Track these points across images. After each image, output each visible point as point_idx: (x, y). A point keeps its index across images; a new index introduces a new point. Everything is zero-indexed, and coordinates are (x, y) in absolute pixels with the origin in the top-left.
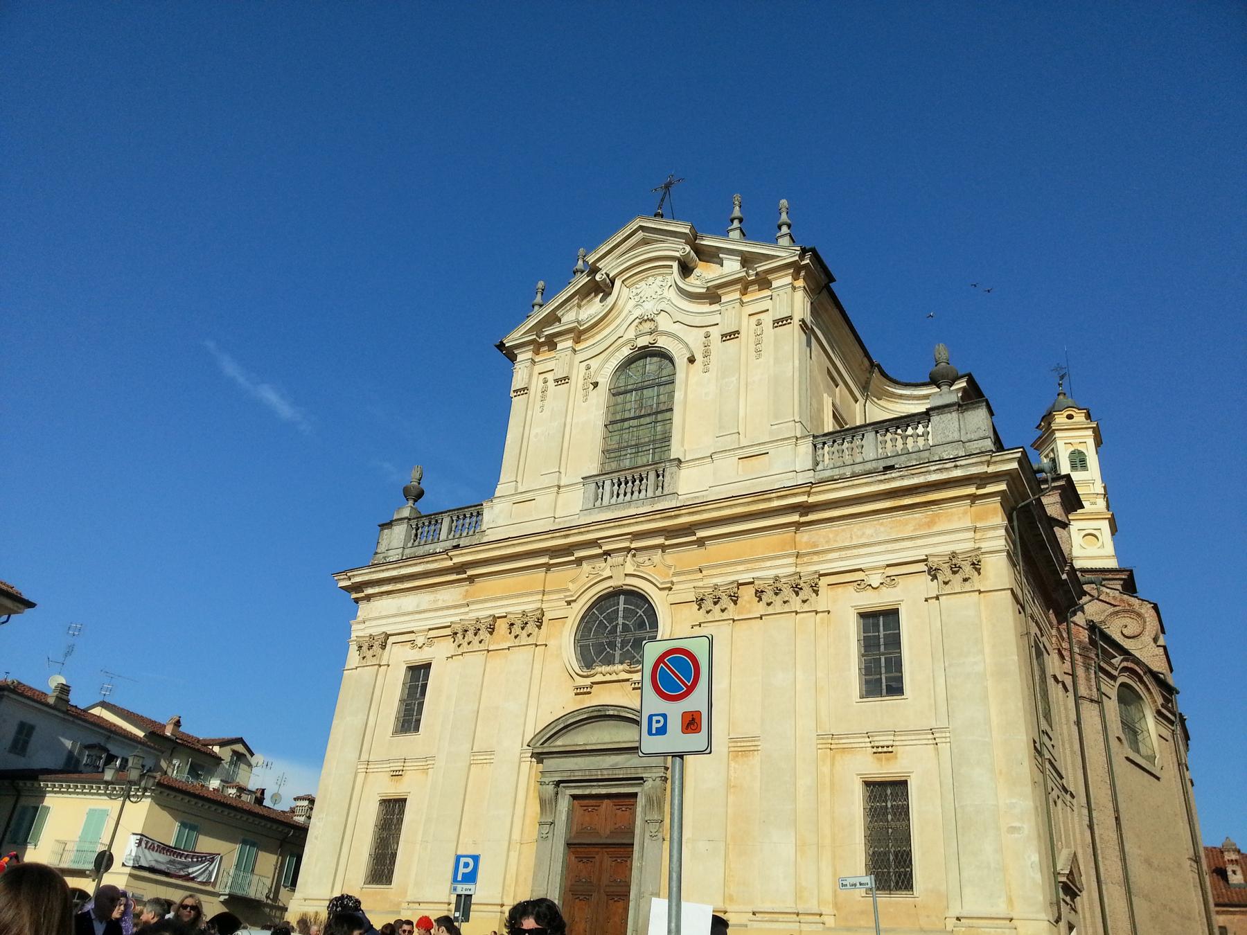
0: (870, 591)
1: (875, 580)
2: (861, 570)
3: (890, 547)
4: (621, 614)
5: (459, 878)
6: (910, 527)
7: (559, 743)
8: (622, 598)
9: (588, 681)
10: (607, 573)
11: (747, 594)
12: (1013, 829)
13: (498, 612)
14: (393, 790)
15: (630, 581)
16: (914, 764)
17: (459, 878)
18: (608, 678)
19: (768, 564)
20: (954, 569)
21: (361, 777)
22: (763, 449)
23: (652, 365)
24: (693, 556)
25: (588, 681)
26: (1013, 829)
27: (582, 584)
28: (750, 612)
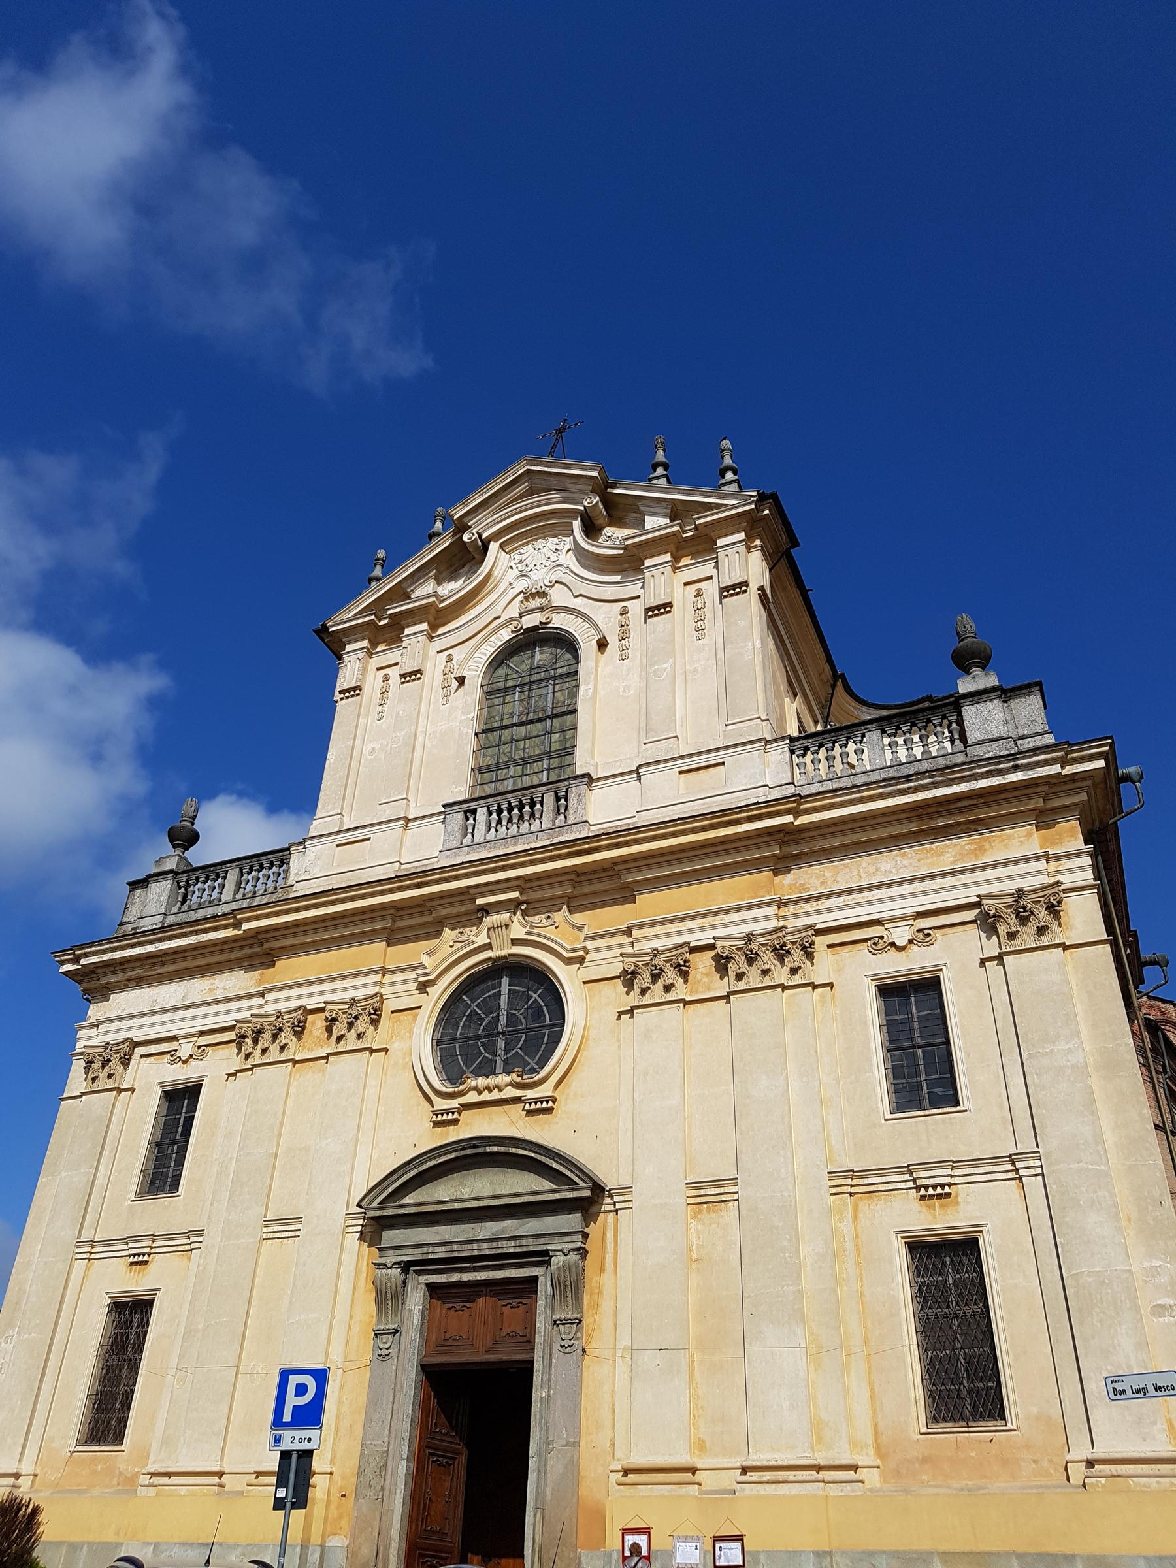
0: (892, 952)
1: (901, 935)
8: (505, 981)
9: (455, 1103)
10: (482, 939)
25: (455, 1103)
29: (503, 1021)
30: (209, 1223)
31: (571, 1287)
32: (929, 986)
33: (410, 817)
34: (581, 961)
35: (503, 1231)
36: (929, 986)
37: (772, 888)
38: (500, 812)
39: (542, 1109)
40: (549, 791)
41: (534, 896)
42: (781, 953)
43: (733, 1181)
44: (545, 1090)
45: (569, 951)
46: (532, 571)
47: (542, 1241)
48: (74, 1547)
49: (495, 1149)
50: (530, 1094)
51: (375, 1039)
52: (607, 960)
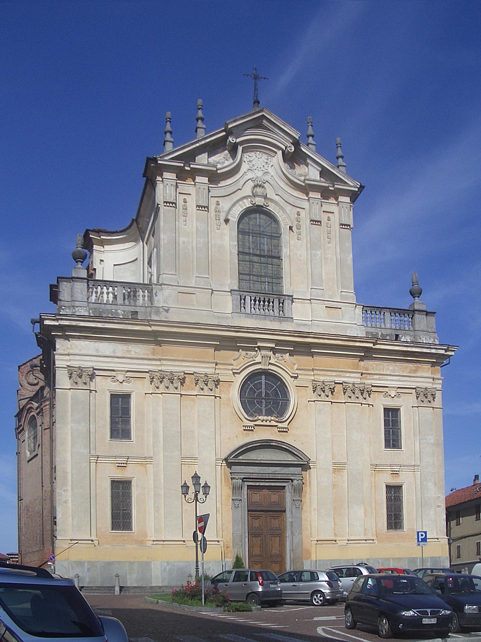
0: (390, 398)
1: (393, 394)
2: (387, 387)
3: (401, 378)
4: (263, 386)
5: (420, 540)
6: (408, 370)
7: (241, 458)
8: (263, 377)
9: (252, 424)
10: (259, 359)
11: (339, 388)
12: (439, 506)
13: (187, 370)
14: (120, 475)
15: (271, 367)
16: (406, 480)
17: (420, 540)
18: (264, 423)
19: (348, 375)
20: (425, 395)
21: (93, 465)
22: (339, 305)
23: (260, 219)
24: (305, 360)
25: (252, 424)
26: (439, 506)
27: (242, 363)
28: (338, 399)
29: (264, 395)
30: (154, 455)
31: (299, 490)
32: (126, 397)
33: (428, 311)
34: (296, 378)
35: (276, 471)
36: (126, 397)
37: (357, 367)
38: (255, 301)
39: (284, 431)
40: (276, 298)
41: (280, 347)
42: (426, 396)
43: (345, 464)
44: (285, 425)
45: (293, 374)
46: (261, 171)
47: (289, 475)
48: (131, 563)
49: (274, 444)
50: (280, 425)
51: (217, 392)
52: (306, 379)
